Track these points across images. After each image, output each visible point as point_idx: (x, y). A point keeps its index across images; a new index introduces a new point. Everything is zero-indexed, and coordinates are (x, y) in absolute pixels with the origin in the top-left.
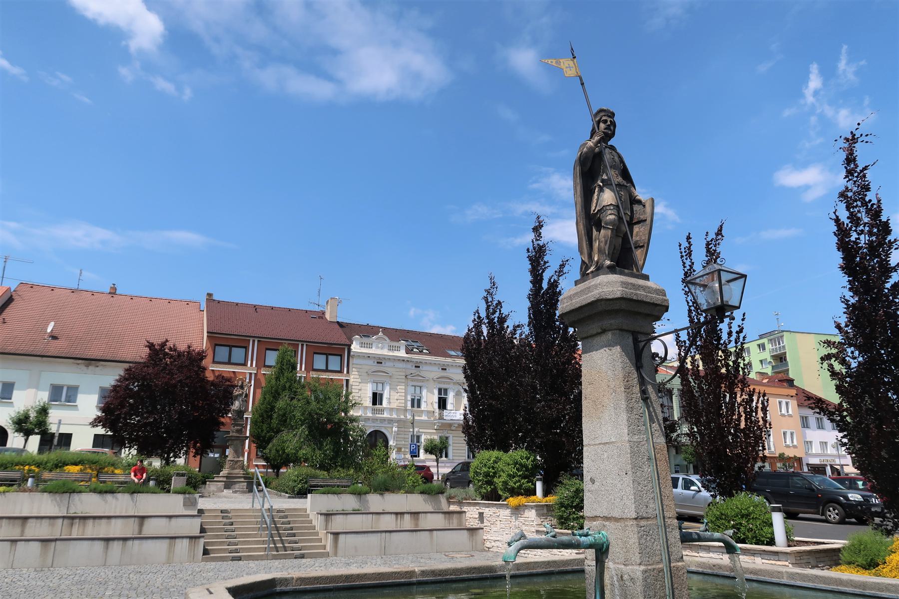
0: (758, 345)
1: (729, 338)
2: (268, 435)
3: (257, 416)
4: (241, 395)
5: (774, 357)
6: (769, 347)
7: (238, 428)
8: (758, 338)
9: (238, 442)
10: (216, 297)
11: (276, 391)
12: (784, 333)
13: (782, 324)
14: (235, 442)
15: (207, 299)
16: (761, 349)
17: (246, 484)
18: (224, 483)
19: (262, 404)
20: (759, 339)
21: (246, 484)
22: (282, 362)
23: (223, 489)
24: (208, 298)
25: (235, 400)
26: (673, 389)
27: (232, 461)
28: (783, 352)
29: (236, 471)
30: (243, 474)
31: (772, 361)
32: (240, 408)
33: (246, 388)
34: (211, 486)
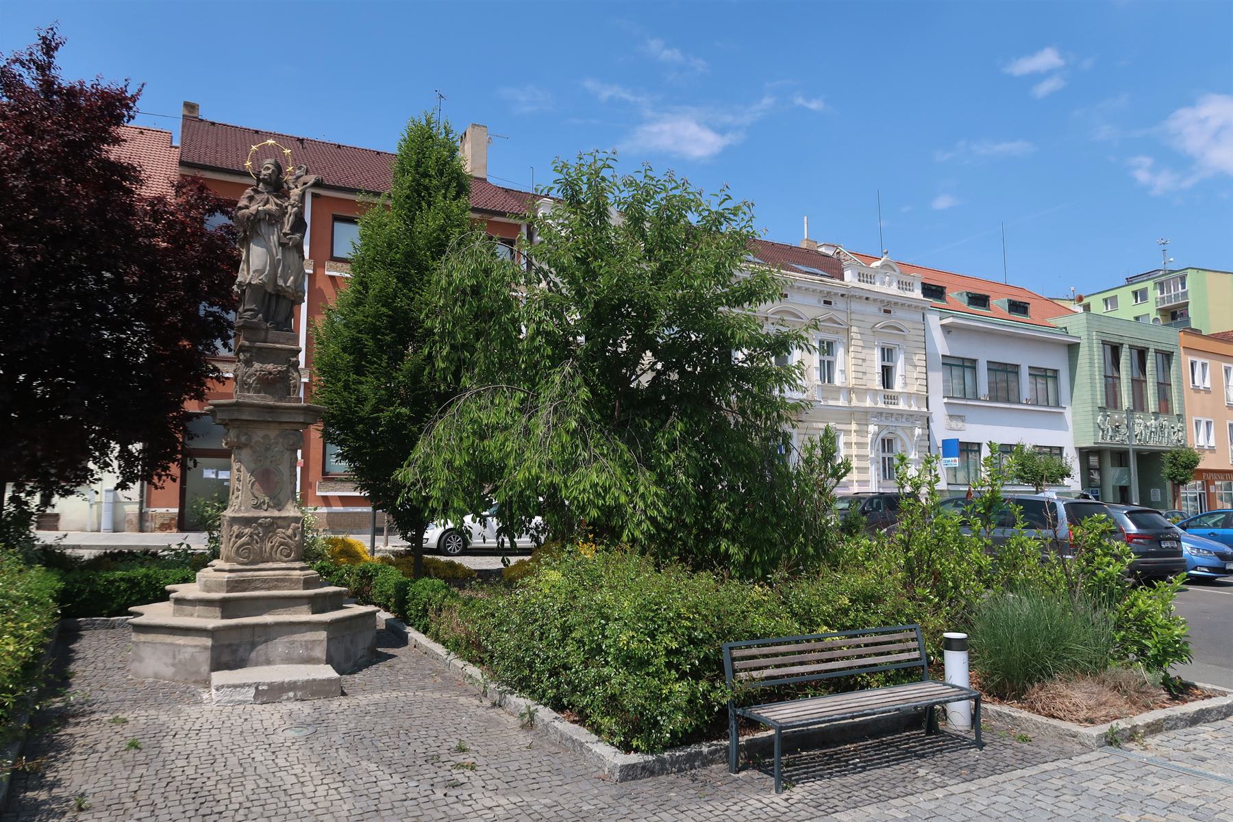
0: (1133, 292)
1: (171, 476)
2: (385, 415)
3: (333, 348)
4: (274, 219)
5: (1163, 312)
6: (1154, 294)
7: (270, 367)
8: (1125, 282)
9: (273, 433)
10: (205, 113)
11: (410, 255)
12: (1188, 271)
13: (1172, 259)
14: (258, 435)
15: (184, 116)
16: (1139, 298)
17: (323, 635)
18: (208, 642)
19: (359, 303)
20: (1126, 285)
21: (323, 635)
22: (419, 164)
23: (205, 668)
24: (186, 113)
25: (246, 241)
26: (1122, 344)
27: (247, 522)
28: (1181, 302)
29: (271, 570)
30: (308, 583)
31: (1159, 317)
32: (273, 277)
33: (295, 193)
34: (146, 652)
